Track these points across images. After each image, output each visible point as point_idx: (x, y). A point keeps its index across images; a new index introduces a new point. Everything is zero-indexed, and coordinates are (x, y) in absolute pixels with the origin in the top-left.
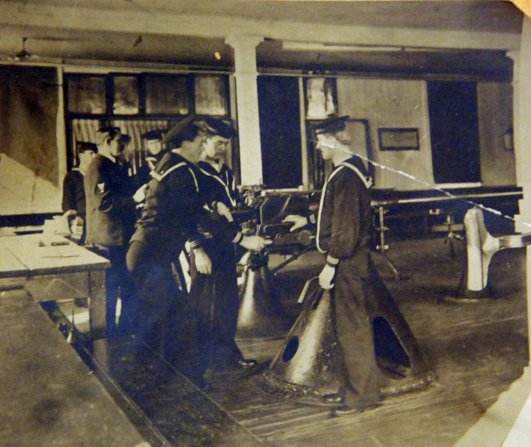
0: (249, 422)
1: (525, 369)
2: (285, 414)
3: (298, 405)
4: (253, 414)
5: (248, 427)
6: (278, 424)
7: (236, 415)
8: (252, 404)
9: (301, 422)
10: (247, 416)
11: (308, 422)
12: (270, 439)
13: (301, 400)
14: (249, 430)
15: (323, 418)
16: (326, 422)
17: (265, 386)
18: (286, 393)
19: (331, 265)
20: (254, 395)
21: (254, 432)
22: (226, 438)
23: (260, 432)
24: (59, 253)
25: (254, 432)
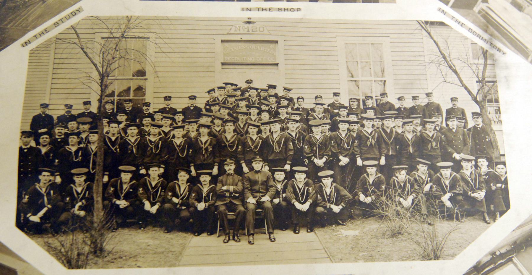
0: (11, 24)
1: (205, 235)
2: (23, 14)
3: (27, 7)
4: (11, 20)
5: (12, 26)
6: (23, 18)
7: (4, 26)
8: (9, 17)
9: (32, 12)
10: (9, 23)
11: (35, 10)
12: (24, 25)
13: (28, 4)
14: (13, 27)
15: (41, 5)
16: (42, 6)
17: (10, 8)
18: (20, 6)
19: (342, 206)
20: (7, 14)
21: (16, 26)
22: (6, 36)
23: (18, 25)
24: (446, 75)
25: (16, 26)
